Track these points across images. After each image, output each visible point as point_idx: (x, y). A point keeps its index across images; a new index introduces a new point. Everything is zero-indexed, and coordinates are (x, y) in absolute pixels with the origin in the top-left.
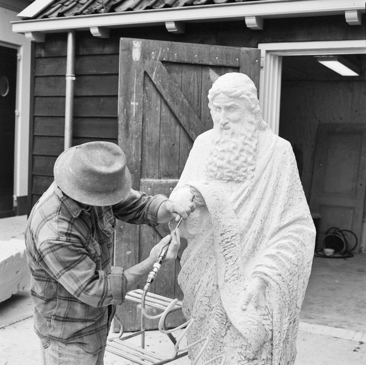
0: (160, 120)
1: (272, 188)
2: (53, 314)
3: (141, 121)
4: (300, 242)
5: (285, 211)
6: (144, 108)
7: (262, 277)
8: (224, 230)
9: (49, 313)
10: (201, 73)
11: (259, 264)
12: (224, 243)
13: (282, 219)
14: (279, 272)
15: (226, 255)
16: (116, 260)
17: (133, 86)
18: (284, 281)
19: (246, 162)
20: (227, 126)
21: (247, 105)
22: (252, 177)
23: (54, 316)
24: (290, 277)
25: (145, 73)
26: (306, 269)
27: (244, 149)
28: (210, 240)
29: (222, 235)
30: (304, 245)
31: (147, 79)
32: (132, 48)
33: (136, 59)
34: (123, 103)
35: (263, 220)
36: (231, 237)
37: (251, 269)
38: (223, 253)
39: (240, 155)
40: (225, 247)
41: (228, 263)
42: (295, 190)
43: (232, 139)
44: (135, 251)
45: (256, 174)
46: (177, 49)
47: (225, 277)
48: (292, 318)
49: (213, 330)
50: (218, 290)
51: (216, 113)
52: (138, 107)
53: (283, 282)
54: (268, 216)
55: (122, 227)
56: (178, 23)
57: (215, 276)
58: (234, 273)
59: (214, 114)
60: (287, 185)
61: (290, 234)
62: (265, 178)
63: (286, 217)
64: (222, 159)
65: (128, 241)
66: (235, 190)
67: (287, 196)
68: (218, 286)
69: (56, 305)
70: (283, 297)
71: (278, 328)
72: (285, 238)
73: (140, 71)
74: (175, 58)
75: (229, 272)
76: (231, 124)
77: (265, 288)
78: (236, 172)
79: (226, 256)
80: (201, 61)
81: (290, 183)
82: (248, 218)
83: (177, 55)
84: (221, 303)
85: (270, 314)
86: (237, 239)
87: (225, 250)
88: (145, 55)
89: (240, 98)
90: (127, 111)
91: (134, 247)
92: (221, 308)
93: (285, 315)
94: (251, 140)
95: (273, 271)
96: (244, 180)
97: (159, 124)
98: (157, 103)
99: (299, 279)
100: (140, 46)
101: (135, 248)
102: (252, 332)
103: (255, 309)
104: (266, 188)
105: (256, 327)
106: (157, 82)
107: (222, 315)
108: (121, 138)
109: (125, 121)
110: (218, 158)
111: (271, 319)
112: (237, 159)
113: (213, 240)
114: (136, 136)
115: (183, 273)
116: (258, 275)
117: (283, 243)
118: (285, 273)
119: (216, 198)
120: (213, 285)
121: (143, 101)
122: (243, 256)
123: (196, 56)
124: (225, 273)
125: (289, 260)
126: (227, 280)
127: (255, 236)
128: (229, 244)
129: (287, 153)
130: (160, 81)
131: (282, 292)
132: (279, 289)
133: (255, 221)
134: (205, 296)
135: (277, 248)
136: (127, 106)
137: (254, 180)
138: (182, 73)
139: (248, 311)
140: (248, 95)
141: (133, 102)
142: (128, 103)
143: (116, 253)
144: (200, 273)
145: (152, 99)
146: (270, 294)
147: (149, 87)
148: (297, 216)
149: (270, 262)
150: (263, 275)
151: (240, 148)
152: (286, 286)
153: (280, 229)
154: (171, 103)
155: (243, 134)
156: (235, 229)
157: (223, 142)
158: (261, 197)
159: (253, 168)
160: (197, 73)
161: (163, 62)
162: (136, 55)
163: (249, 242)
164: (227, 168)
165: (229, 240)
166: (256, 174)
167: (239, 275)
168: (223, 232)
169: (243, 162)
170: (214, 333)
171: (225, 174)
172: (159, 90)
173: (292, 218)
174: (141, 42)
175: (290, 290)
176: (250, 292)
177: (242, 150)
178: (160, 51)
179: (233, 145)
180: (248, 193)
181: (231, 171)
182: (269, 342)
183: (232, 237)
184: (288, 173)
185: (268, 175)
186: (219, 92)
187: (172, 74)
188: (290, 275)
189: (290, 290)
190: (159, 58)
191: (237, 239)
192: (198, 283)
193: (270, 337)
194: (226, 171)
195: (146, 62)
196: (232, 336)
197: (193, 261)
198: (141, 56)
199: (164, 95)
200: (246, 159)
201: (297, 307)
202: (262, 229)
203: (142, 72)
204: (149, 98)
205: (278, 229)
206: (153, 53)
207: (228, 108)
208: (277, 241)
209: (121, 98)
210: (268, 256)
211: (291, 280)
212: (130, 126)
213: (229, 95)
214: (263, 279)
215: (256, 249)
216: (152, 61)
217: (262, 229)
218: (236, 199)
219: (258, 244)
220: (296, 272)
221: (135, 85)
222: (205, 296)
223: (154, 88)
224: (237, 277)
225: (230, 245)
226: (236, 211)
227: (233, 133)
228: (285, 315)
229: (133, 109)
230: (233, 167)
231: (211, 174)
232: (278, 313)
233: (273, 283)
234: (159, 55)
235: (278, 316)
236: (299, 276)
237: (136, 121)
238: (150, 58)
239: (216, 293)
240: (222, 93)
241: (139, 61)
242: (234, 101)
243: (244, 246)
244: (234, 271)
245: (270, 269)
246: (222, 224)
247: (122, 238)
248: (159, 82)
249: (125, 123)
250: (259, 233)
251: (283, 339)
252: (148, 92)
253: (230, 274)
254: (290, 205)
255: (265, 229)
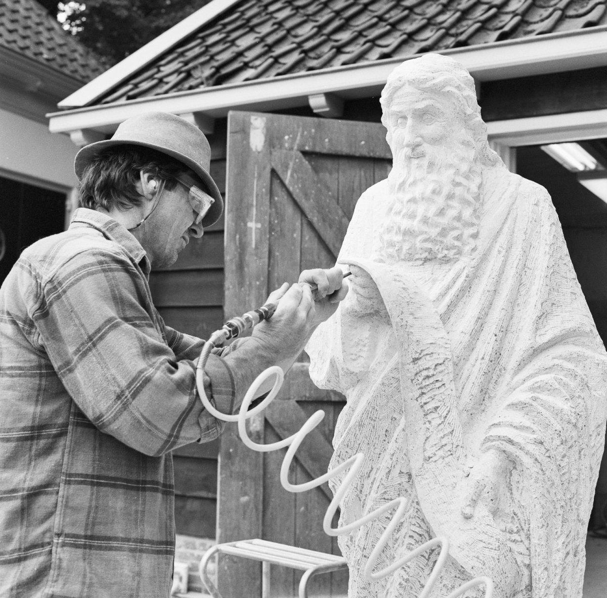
0: (301, 256)
1: (514, 270)
2: (56, 531)
3: (267, 255)
4: (579, 379)
5: (544, 315)
6: (272, 230)
7: (503, 447)
8: (419, 351)
9: (44, 533)
10: (372, 172)
11: (496, 422)
12: (421, 379)
13: (538, 333)
14: (538, 436)
15: (425, 404)
16: (221, 513)
17: (251, 194)
18: (549, 457)
19: (458, 218)
20: (419, 149)
21: (458, 108)
22: (474, 250)
23: (59, 535)
24: (561, 450)
25: (273, 172)
26: (593, 438)
27: (454, 194)
28: (392, 381)
29: (415, 360)
30: (588, 387)
31: (276, 182)
32: (250, 128)
33: (256, 147)
34: (233, 224)
35: (500, 333)
36: (433, 367)
37: (479, 433)
38: (419, 399)
39: (447, 205)
40: (421, 388)
41: (430, 422)
42: (563, 277)
43: (429, 176)
44: (256, 495)
45: (481, 244)
46: (329, 130)
47: (425, 450)
48: (571, 542)
49: (403, 572)
50: (411, 483)
51: (396, 129)
52: (261, 232)
53: (549, 459)
54: (509, 328)
55: (231, 450)
56: (330, 96)
57: (405, 454)
58: (444, 442)
59: (394, 132)
60: (545, 265)
61: (556, 362)
62: (499, 252)
63: (546, 329)
64: (412, 216)
65: (242, 476)
66: (439, 278)
67: (547, 285)
68: (410, 476)
69: (56, 504)
70: (549, 492)
71: (543, 558)
72: (547, 370)
73: (264, 168)
74: (325, 146)
75: (431, 441)
76: (426, 148)
77: (511, 475)
78: (441, 239)
79: (427, 407)
80: (373, 151)
81: (552, 260)
82: (469, 330)
83: (329, 141)
84: (418, 510)
85: (523, 529)
86: (446, 371)
87: (423, 393)
88: (272, 141)
89: (444, 94)
90: (240, 240)
91: (253, 489)
92: (419, 521)
93: (557, 533)
94: (467, 177)
95: (523, 434)
96: (457, 256)
97: (299, 262)
98: (294, 225)
99: (580, 457)
100: (263, 125)
101: (256, 490)
102: (487, 565)
103: (491, 517)
104: (502, 272)
105: (494, 554)
106: (293, 187)
107: (420, 535)
108: (231, 287)
109: (238, 255)
110: (403, 216)
111: (527, 542)
112: (441, 212)
113: (398, 380)
114: (258, 283)
115: (338, 458)
116: (494, 443)
117: (543, 379)
118: (550, 441)
119: (401, 284)
120: (401, 473)
121: (270, 222)
122: (461, 408)
123: (363, 143)
124: (425, 443)
125: (558, 413)
126: (430, 458)
127: (484, 366)
128: (431, 380)
129: (541, 204)
130: (300, 186)
131: (546, 479)
132: (541, 472)
133: (482, 338)
134: (384, 499)
135: (532, 389)
136: (241, 230)
137: (477, 255)
138: (338, 172)
139: (475, 519)
140: (458, 87)
141: (251, 221)
142: (242, 224)
143: (221, 500)
144: (372, 453)
145: (286, 218)
146: (520, 486)
147: (281, 197)
148: (569, 325)
149: (518, 417)
150: (504, 443)
151: (447, 193)
152: (555, 468)
153: (536, 352)
154: (320, 224)
155: (451, 166)
156: (442, 350)
157: (414, 183)
158: (493, 289)
159: (476, 231)
160: (365, 173)
161: (305, 153)
162: (257, 140)
163: (472, 379)
164: (422, 233)
165: (431, 372)
166: (481, 244)
167: (454, 446)
168: (417, 356)
169: (454, 219)
170: (406, 577)
171: (418, 245)
172: (298, 200)
173: (559, 329)
174: (264, 119)
175: (563, 479)
176: (479, 477)
177: (450, 197)
178: (299, 134)
179: (431, 187)
180: (465, 280)
181: (429, 238)
182: (524, 592)
183: (436, 365)
184: (546, 240)
185: (505, 246)
186: (402, 83)
187: (321, 175)
188: (562, 444)
189: (563, 479)
190: (298, 147)
191: (446, 371)
192: (369, 477)
193: (526, 580)
194: (420, 238)
195: (274, 153)
196: (445, 582)
197: (357, 429)
198: (265, 143)
199: (307, 211)
200: (460, 213)
201: (579, 521)
202: (498, 354)
203: (268, 170)
204: (280, 216)
205: (531, 351)
206: (286, 137)
207: (422, 115)
208: (531, 376)
209: (230, 215)
210: (513, 406)
211: (564, 456)
212: (247, 265)
213: (422, 86)
214: (504, 451)
215: (487, 396)
216: (284, 151)
217: (498, 354)
218: (443, 295)
219: (491, 386)
220: (573, 440)
221: (255, 192)
222: (384, 499)
223: (290, 199)
224: (450, 451)
225: (433, 383)
226: (445, 318)
227: (431, 165)
228: (557, 533)
229: (251, 235)
230: (433, 230)
231: (391, 250)
232: (541, 525)
233: (526, 460)
234: (297, 142)
235: (542, 532)
236: (580, 452)
237: (256, 255)
238: (281, 146)
239: (406, 491)
240: (407, 85)
241: (262, 151)
242: (431, 98)
243: (463, 388)
244: (442, 438)
245: (518, 431)
246: (414, 339)
247: (231, 472)
248: (298, 187)
249: (237, 259)
250: (491, 361)
251: (554, 586)
252: (279, 205)
253: (435, 445)
254: (553, 304)
255: (505, 354)
